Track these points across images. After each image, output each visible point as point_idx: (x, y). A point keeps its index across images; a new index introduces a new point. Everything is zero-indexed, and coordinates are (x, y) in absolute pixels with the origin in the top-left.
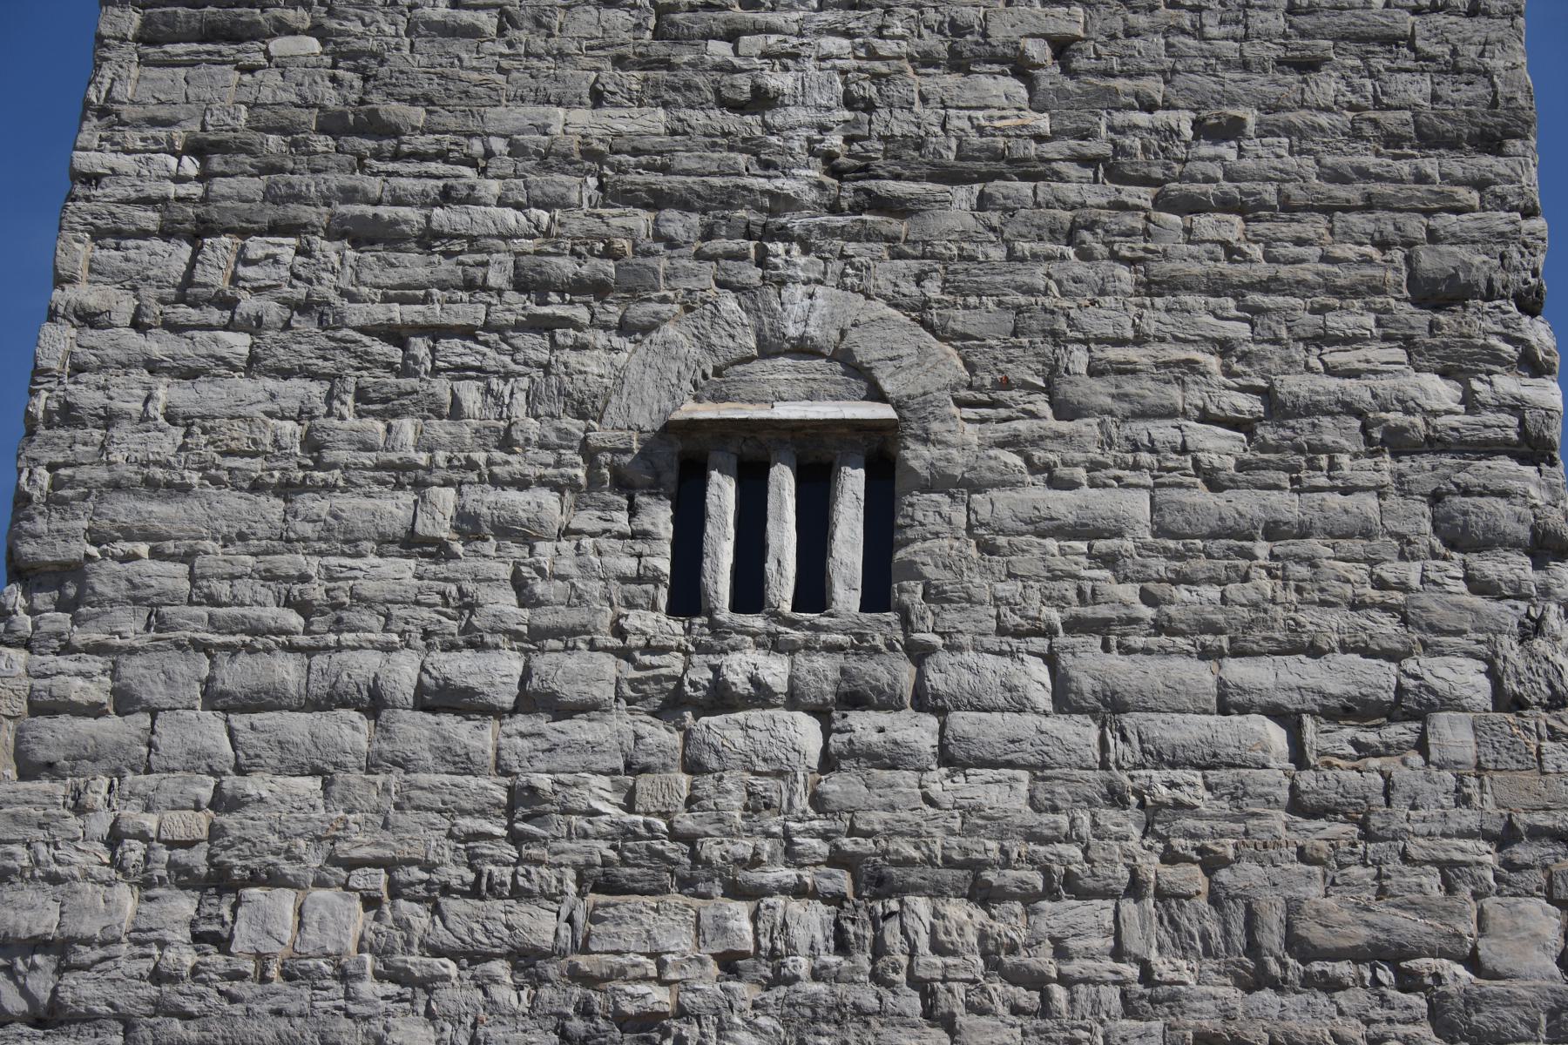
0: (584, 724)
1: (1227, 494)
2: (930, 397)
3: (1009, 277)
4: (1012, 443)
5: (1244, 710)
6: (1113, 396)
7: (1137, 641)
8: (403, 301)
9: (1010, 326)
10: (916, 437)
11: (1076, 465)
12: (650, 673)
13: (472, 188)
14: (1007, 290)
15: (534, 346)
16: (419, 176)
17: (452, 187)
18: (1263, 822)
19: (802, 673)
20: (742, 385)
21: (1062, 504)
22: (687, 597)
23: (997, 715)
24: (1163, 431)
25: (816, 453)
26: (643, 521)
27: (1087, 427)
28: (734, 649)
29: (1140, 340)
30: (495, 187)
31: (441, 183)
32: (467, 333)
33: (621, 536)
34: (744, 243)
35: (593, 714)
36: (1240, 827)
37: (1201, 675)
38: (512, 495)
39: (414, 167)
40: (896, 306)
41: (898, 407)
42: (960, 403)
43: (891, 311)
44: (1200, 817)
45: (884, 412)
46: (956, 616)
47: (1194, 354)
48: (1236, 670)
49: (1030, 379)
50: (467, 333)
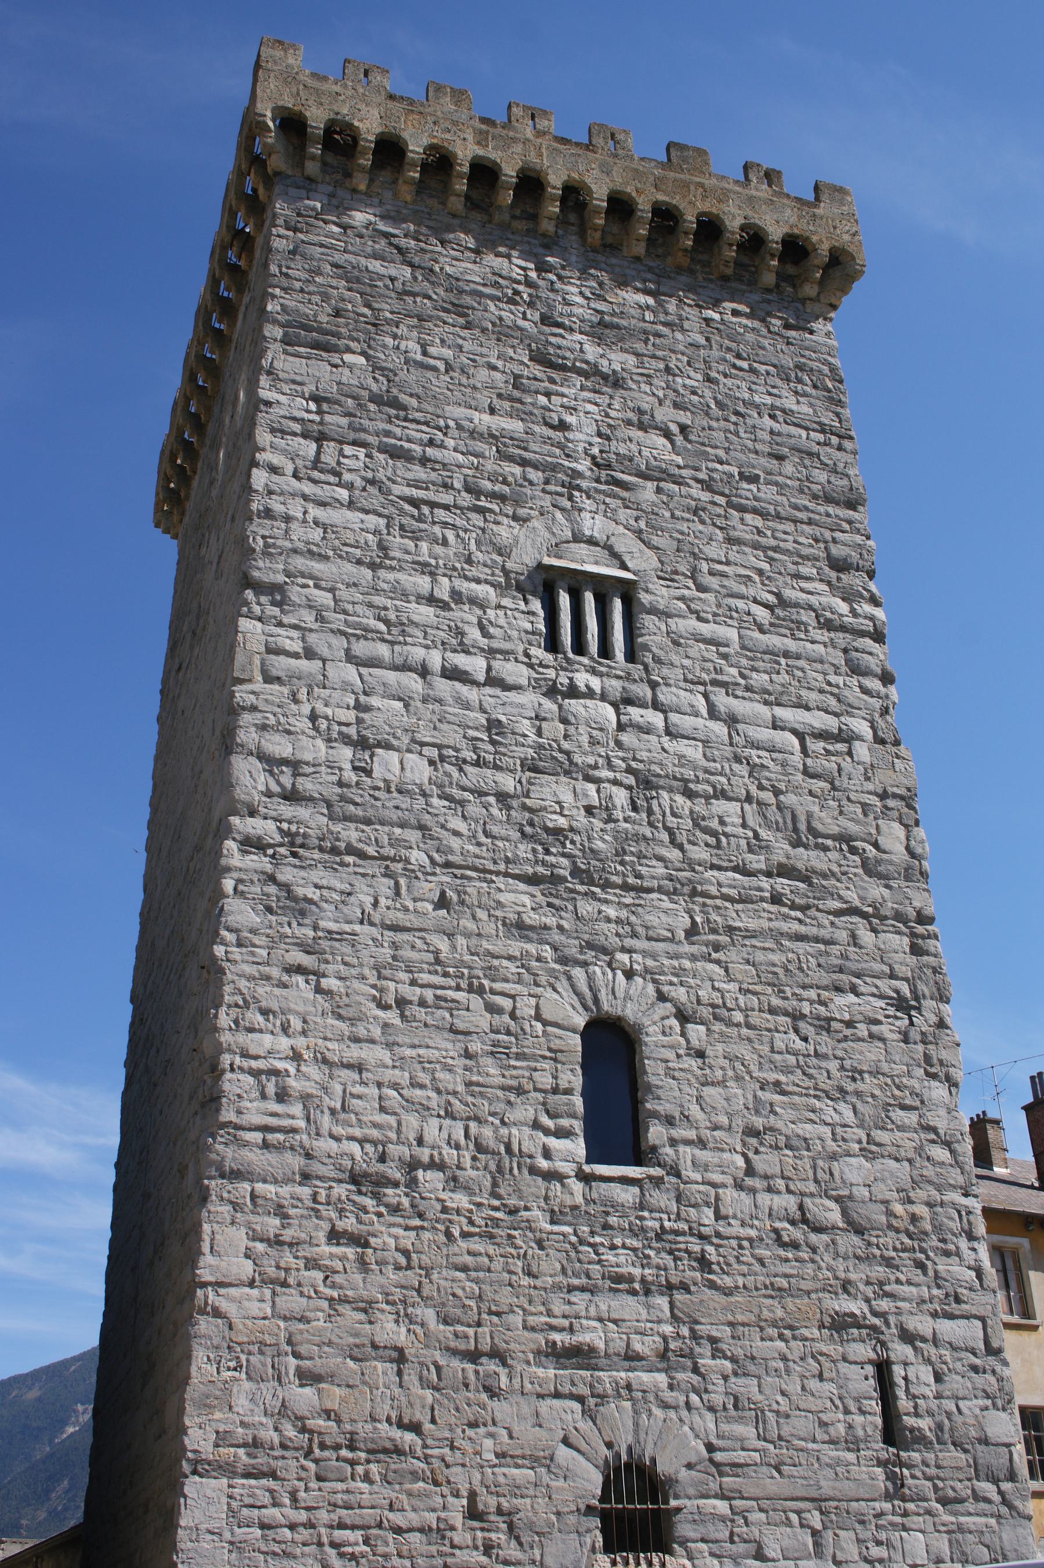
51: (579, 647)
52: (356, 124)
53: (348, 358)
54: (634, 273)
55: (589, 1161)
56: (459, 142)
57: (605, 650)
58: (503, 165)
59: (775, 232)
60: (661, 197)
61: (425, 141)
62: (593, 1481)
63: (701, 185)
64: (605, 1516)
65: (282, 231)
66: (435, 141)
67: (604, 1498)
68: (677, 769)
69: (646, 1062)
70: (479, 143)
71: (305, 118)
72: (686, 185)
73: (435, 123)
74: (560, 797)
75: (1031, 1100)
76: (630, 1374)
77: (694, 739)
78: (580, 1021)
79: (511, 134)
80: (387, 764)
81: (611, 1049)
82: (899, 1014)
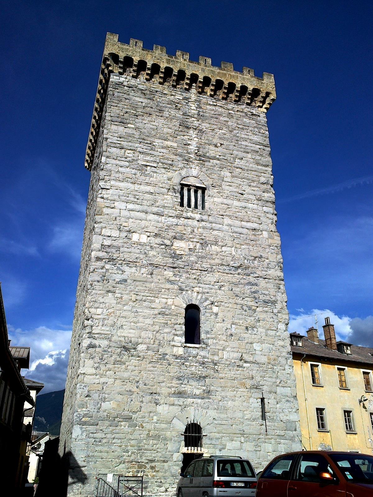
7: (232, 218)
16: (148, 146)
21: (225, 201)
51: (189, 205)
52: (133, 58)
53: (129, 125)
54: (210, 100)
55: (186, 343)
56: (162, 63)
57: (196, 207)
58: (174, 69)
59: (250, 88)
60: (218, 78)
61: (152, 63)
62: (183, 428)
63: (230, 75)
64: (186, 437)
65: (111, 89)
66: (155, 62)
67: (185, 432)
68: (265, 106)
69: (83, 469)
70: (167, 63)
71: (119, 56)
72: (225, 74)
73: (155, 57)
74: (180, 246)
75: (325, 324)
76: (194, 400)
77: (220, 230)
78: (185, 306)
79: (177, 60)
80: (135, 237)
81: (192, 315)
82: (272, 305)
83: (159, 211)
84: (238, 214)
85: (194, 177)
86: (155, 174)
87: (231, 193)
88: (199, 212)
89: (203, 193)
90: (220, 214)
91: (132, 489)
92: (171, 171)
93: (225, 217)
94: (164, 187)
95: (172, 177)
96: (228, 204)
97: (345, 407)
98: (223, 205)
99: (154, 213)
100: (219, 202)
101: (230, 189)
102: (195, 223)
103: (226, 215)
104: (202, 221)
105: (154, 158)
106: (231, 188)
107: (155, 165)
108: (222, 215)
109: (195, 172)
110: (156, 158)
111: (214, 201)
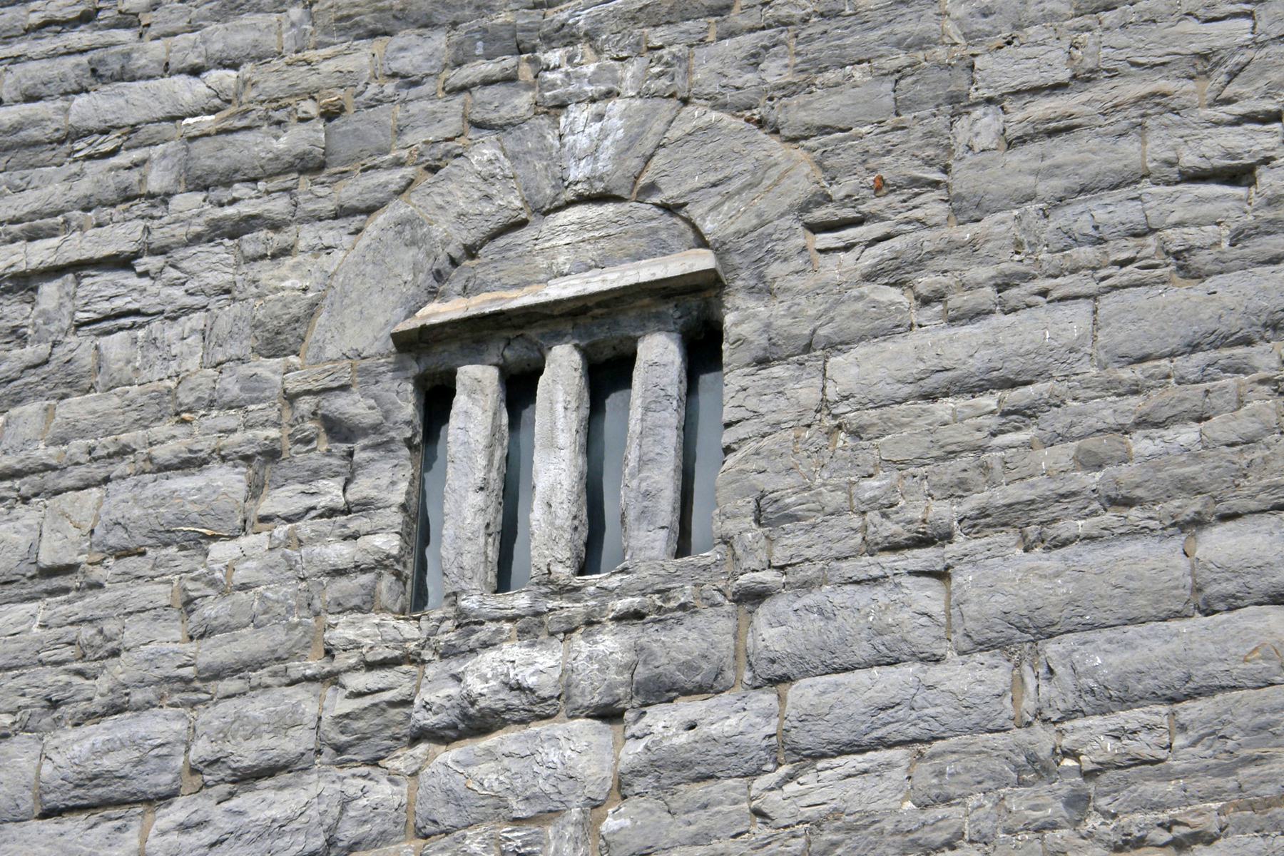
0: (271, 795)
1: (1211, 283)
2: (769, 229)
3: (885, 29)
4: (894, 273)
5: (1232, 603)
6: (1036, 173)
7: (1067, 527)
8: (32, 236)
9: (888, 102)
10: (751, 290)
11: (980, 285)
12: (367, 701)
13: (127, 55)
14: (883, 50)
15: (214, 265)
16: (53, 55)
17: (102, 62)
18: (1266, 769)
19: (580, 663)
20: (506, 264)
21: (966, 347)
22: (413, 579)
23: (860, 676)
24: (1115, 211)
25: (603, 335)
26: (362, 488)
27: (996, 226)
28: (486, 645)
29: (1084, 78)
30: (157, 49)
31: (84, 59)
32: (122, 262)
33: (331, 512)
34: (510, 61)
35: (283, 778)
36: (1230, 783)
37: (1156, 560)
38: (181, 483)
39: (49, 43)
40: (723, 107)
41: (721, 250)
42: (816, 228)
43: (714, 115)
44: (1168, 776)
45: (703, 261)
46: (802, 539)
47: (1161, 83)
48: (1219, 543)
49: (917, 173)
50: (122, 262)
83: (108, 763)
84: (1141, 444)
85: (582, 199)
86: (115, 345)
87: (1061, 218)
88: (621, 593)
89: (703, 350)
90: (891, 529)
91: (1264, 201)
92: (307, 235)
93: (961, 543)
94: (205, 445)
95: (314, 307)
96: (1011, 368)
97: (567, 484)
98: (944, 407)
99: (53, 799)
100: (885, 390)
101: (1051, 172)
102: (579, 749)
103: (980, 521)
104: (660, 691)
105: (123, 159)
106: (1063, 151)
107: (121, 235)
108: (922, 541)
109: (591, 139)
110: (136, 155)
111: (832, 394)
